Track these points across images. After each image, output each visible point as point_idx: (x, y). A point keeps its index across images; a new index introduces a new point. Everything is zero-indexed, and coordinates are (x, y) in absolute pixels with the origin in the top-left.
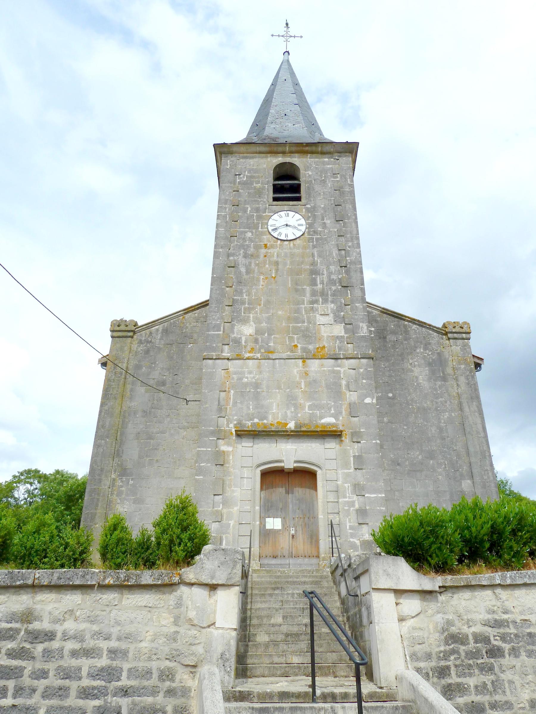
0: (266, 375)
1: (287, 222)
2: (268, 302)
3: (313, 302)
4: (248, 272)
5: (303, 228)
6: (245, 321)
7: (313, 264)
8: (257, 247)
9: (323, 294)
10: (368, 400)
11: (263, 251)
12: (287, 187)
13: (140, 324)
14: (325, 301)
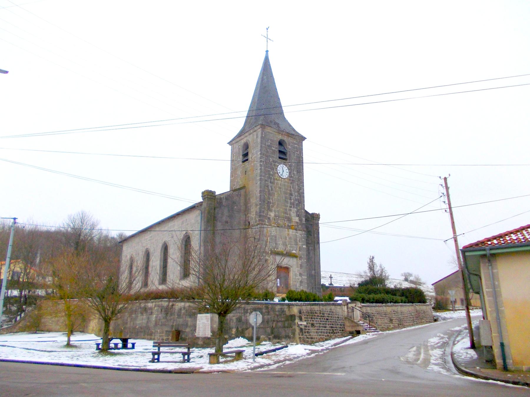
0: (278, 233)
1: (283, 171)
2: (278, 204)
3: (291, 207)
4: (272, 190)
5: (282, 165)
6: (271, 211)
7: (291, 191)
8: (274, 179)
9: (294, 205)
10: (304, 246)
11: (276, 181)
12: (283, 155)
13: (222, 186)
14: (294, 207)
